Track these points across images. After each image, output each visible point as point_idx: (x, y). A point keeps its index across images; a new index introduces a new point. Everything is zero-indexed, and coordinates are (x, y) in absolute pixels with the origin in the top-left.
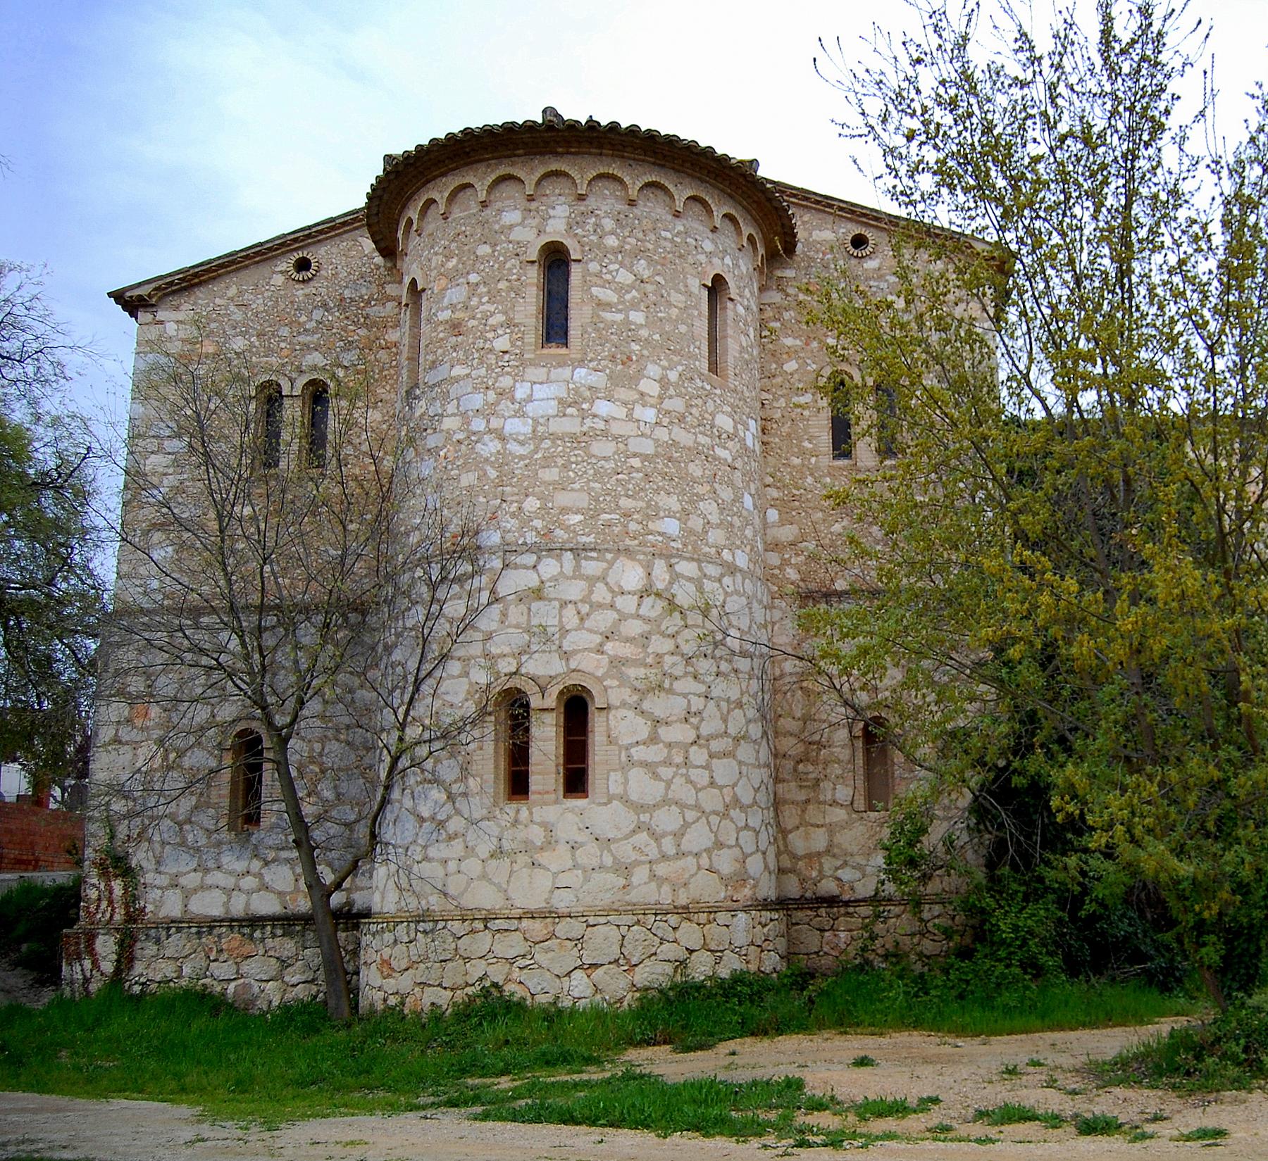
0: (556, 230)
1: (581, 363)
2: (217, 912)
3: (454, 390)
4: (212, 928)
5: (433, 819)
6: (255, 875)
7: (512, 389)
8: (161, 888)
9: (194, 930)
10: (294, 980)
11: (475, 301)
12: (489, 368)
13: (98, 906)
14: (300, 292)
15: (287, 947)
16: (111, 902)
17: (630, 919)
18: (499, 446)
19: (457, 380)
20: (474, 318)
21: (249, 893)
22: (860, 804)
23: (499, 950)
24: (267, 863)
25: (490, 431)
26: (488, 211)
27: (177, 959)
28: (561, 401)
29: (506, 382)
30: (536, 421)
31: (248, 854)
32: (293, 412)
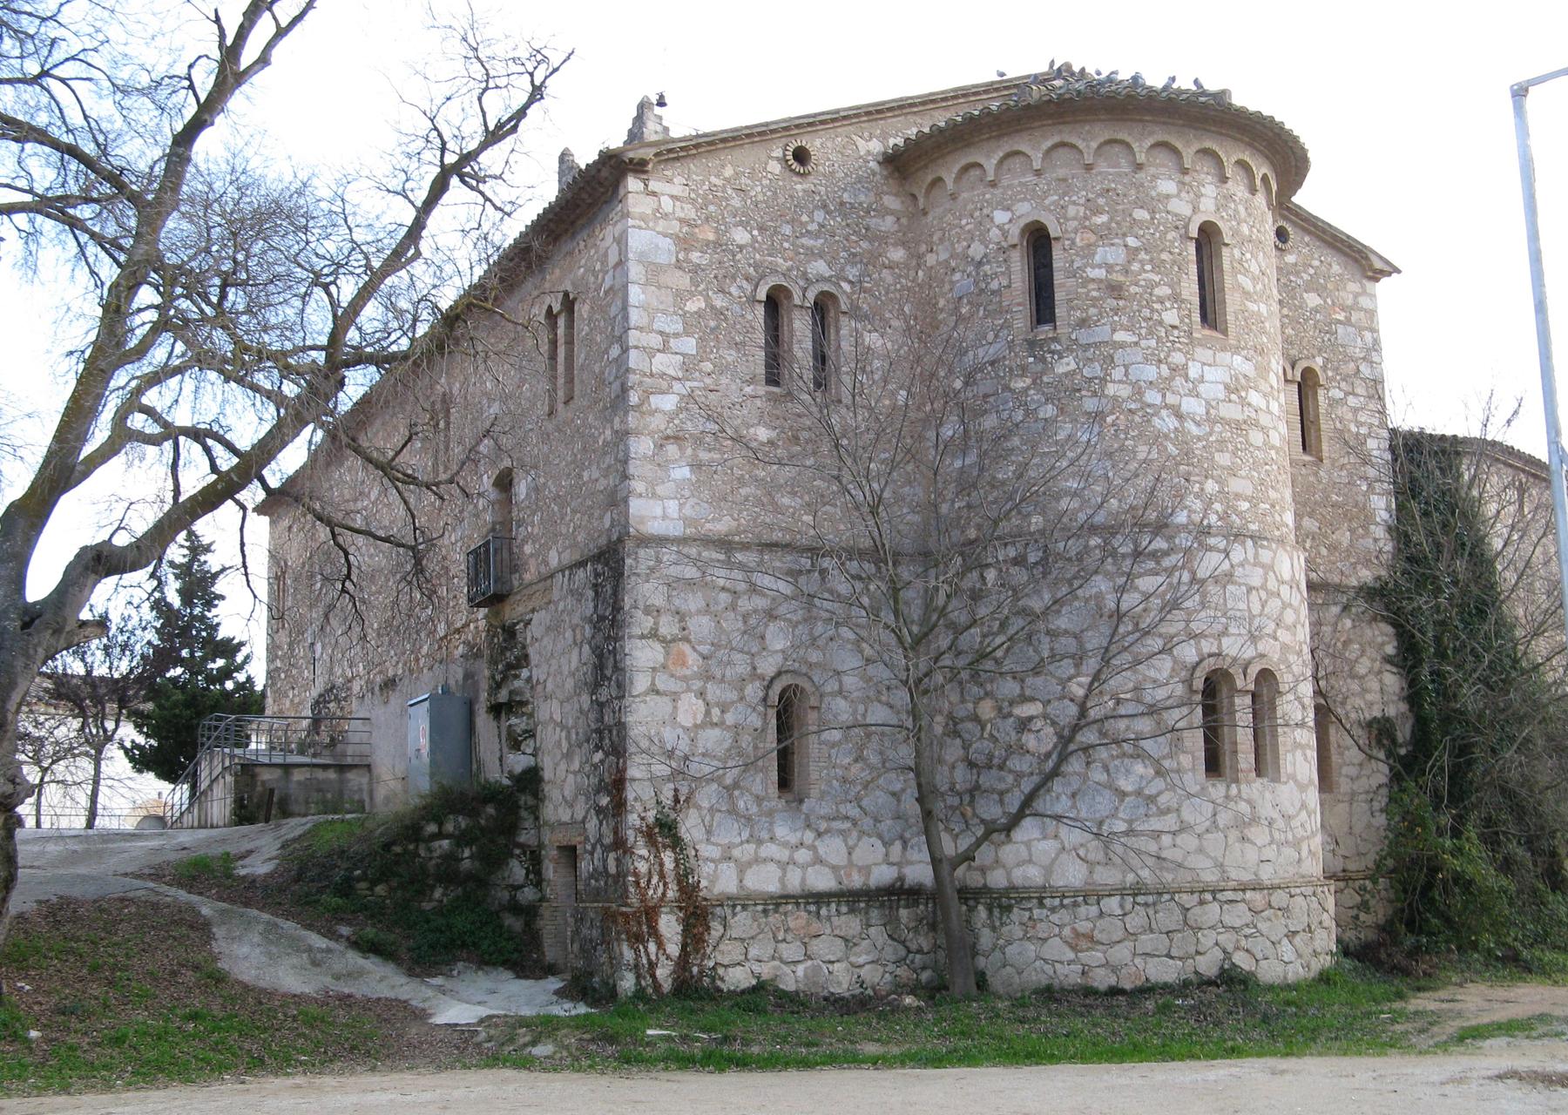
0: (1208, 210)
1: (1236, 350)
2: (773, 887)
3: (1118, 355)
4: (778, 905)
5: (1139, 793)
6: (808, 848)
7: (1185, 367)
8: (713, 861)
9: (760, 908)
10: (861, 960)
11: (1135, 267)
12: (1159, 339)
13: (649, 881)
14: (800, 187)
15: (850, 924)
16: (662, 876)
17: (1309, 891)
18: (1177, 424)
19: (1122, 345)
20: (1136, 284)
21: (804, 867)
23: (1227, 920)
24: (819, 835)
25: (1166, 406)
26: (1141, 175)
27: (742, 940)
28: (1227, 387)
29: (1177, 358)
30: (1208, 403)
31: (800, 823)
32: (800, 327)
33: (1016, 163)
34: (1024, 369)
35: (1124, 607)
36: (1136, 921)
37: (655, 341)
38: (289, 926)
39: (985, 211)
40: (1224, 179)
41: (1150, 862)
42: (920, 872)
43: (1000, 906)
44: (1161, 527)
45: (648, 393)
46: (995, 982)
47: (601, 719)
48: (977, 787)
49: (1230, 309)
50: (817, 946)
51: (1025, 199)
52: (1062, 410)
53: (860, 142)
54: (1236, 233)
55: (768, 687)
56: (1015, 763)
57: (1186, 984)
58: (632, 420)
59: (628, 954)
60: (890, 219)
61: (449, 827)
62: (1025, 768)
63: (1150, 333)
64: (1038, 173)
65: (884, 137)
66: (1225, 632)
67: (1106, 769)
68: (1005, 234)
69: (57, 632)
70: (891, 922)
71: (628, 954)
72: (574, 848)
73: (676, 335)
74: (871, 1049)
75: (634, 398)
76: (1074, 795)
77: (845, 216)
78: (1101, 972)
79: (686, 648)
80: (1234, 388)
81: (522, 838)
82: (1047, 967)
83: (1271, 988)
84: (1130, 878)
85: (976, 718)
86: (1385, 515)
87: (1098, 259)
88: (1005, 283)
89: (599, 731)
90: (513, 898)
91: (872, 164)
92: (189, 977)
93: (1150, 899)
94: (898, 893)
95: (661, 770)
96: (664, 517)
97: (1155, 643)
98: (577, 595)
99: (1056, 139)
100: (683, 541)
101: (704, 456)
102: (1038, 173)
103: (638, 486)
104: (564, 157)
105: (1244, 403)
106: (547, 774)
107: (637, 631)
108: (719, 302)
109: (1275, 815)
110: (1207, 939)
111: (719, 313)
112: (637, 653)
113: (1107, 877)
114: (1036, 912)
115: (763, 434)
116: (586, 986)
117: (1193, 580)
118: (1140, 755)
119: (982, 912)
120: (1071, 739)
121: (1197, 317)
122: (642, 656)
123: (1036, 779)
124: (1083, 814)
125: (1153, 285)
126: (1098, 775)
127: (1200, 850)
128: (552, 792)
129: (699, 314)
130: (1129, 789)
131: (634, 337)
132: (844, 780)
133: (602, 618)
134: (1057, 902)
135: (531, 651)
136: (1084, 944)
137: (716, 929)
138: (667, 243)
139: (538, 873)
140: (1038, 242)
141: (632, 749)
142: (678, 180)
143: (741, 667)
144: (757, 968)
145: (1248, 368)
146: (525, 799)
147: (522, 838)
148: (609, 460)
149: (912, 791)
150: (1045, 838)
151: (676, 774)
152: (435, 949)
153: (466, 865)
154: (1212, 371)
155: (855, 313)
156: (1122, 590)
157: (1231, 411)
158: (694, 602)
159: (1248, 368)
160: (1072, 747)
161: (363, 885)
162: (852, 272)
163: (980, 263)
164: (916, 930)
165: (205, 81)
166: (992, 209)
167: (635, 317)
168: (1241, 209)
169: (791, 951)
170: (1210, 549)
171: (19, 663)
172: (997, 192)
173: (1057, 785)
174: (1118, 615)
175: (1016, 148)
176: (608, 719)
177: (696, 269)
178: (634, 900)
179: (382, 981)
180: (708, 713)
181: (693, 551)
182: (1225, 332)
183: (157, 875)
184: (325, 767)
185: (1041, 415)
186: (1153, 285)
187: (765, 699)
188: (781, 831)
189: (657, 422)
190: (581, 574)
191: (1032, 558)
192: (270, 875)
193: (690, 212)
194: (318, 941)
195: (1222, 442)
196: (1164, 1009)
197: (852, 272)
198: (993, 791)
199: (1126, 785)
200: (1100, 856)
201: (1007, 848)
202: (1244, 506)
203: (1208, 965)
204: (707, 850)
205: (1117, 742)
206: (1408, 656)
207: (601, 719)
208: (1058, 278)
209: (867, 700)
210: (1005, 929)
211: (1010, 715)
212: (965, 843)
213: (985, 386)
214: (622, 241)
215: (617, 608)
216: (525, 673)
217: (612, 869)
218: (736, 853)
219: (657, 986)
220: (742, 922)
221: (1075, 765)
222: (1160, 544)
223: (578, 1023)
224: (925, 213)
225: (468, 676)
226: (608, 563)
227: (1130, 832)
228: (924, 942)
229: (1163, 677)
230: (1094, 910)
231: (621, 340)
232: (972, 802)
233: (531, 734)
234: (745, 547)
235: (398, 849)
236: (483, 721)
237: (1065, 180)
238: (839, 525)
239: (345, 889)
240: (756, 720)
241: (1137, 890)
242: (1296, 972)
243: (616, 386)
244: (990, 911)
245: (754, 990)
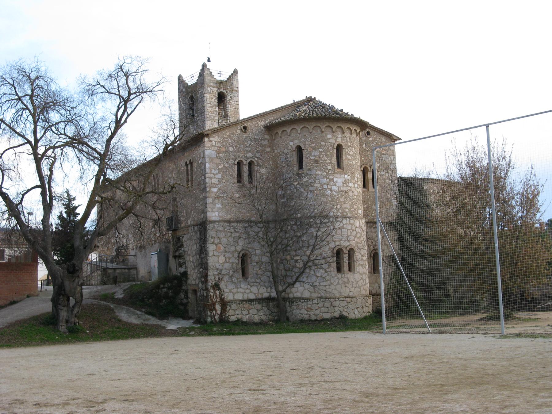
0: (339, 140)
1: (346, 174)
2: (241, 298)
5: (321, 276)
10: (261, 314)
11: (321, 156)
15: (259, 306)
16: (216, 296)
17: (362, 298)
19: (318, 175)
21: (248, 294)
22: (373, 272)
23: (341, 304)
24: (251, 286)
26: (323, 134)
28: (343, 183)
29: (331, 177)
31: (247, 283)
32: (245, 169)
33: (294, 131)
34: (296, 180)
35: (318, 235)
36: (321, 305)
37: (212, 176)
38: (131, 309)
40: (344, 133)
41: (324, 292)
42: (274, 294)
44: (327, 216)
45: (211, 188)
46: (291, 319)
47: (202, 261)
48: (287, 275)
49: (344, 164)
50: (251, 311)
53: (259, 123)
54: (347, 145)
55: (239, 254)
57: (332, 318)
58: (207, 195)
59: (209, 313)
60: (266, 141)
61: (166, 286)
63: (325, 171)
64: (299, 134)
65: (265, 121)
66: (341, 240)
67: (314, 271)
68: (292, 147)
69: (91, 249)
70: (268, 306)
71: (209, 313)
72: (196, 290)
73: (217, 174)
74: (260, 331)
75: (208, 189)
77: (256, 142)
79: (220, 245)
80: (345, 183)
81: (183, 288)
83: (351, 319)
84: (319, 295)
85: (286, 259)
86: (396, 203)
89: (202, 264)
90: (181, 302)
91: (262, 128)
92: (113, 320)
94: (269, 299)
95: (216, 273)
96: (215, 216)
97: (325, 243)
98: (196, 232)
99: (303, 126)
100: (219, 221)
101: (224, 202)
102: (299, 134)
103: (209, 209)
104: (181, 80)
105: (347, 186)
106: (189, 273)
107: (210, 242)
108: (226, 165)
109: (353, 281)
110: (336, 309)
111: (227, 168)
113: (314, 295)
115: (237, 195)
116: (199, 321)
117: (334, 228)
118: (322, 268)
119: (288, 303)
120: (306, 264)
121: (336, 167)
122: (211, 248)
123: (299, 273)
125: (325, 160)
126: (312, 272)
127: (335, 289)
128: (190, 278)
129: (222, 168)
131: (207, 175)
132: (257, 274)
133: (202, 239)
135: (184, 244)
136: (309, 310)
137: (228, 308)
138: (214, 153)
139: (187, 296)
140: (299, 150)
141: (209, 268)
143: (233, 249)
144: (237, 316)
145: (349, 178)
146: (184, 279)
147: (183, 288)
148: (202, 202)
149: (272, 277)
151: (219, 273)
152: (165, 315)
153: (170, 294)
154: (339, 180)
155: (258, 165)
156: (317, 231)
157: (345, 189)
158: (222, 235)
159: (349, 178)
161: (146, 300)
162: (258, 155)
163: (286, 154)
164: (274, 307)
165: (113, 126)
166: (290, 141)
167: (207, 170)
168: (348, 139)
169: (245, 312)
170: (338, 221)
171: (84, 256)
173: (304, 275)
174: (317, 237)
176: (204, 261)
177: (221, 158)
178: (210, 302)
179: (154, 321)
180: (226, 260)
181: (222, 224)
182: (343, 170)
183: (95, 298)
184: (125, 269)
186: (325, 160)
187: (238, 256)
188: (242, 286)
189: (213, 195)
190: (196, 228)
191: (298, 224)
192: (123, 298)
193: (219, 145)
194: (139, 313)
195: (342, 196)
196: (325, 324)
197: (258, 155)
198: (290, 276)
199: (319, 275)
200: (313, 291)
202: (347, 210)
203: (337, 315)
204: (226, 290)
205: (317, 265)
206: (401, 240)
207: (202, 261)
208: (304, 158)
209: (262, 256)
212: (284, 287)
213: (288, 183)
214: (204, 152)
215: (205, 237)
216: (183, 249)
217: (205, 294)
218: (232, 291)
219: (215, 320)
220: (234, 306)
221: (307, 270)
222: (326, 220)
223: (198, 328)
225: (166, 247)
226: (203, 226)
227: (320, 285)
228: (276, 310)
229: (327, 250)
230: (311, 302)
231: (205, 175)
232: (286, 279)
233: (184, 263)
234: (233, 222)
235: (154, 291)
236: (171, 259)
239: (142, 300)
240: (235, 260)
241: (321, 298)
242: (358, 316)
243: (203, 186)
245: (237, 321)
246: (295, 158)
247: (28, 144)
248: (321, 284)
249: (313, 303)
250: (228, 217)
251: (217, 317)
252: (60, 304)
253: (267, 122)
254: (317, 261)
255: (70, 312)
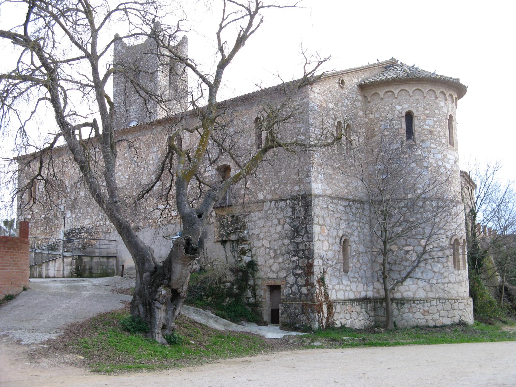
5: (439, 272)
11: (436, 126)
15: (358, 308)
16: (322, 295)
19: (433, 148)
39: (393, 105)
43: (401, 303)
51: (406, 104)
52: (417, 165)
56: (404, 263)
57: (452, 325)
62: (407, 264)
64: (411, 97)
65: (358, 78)
67: (431, 265)
76: (422, 272)
78: (431, 321)
82: (416, 320)
84: (437, 296)
87: (427, 123)
88: (400, 127)
91: (356, 86)
93: (444, 301)
94: (366, 300)
99: (416, 88)
102: (411, 97)
112: (315, 229)
113: (431, 295)
114: (412, 305)
119: (394, 305)
124: (425, 278)
125: (439, 132)
130: (437, 271)
134: (419, 302)
136: (426, 314)
139: (255, 294)
140: (409, 117)
142: (318, 88)
150: (414, 284)
160: (421, 259)
163: (391, 120)
172: (398, 100)
173: (417, 270)
175: (404, 88)
185: (411, 166)
186: (439, 132)
198: (397, 271)
200: (430, 290)
201: (402, 287)
203: (456, 320)
204: (330, 287)
205: (434, 258)
210: (402, 310)
211: (402, 249)
216: (246, 231)
221: (422, 264)
224: (369, 102)
230: (429, 304)
233: (250, 250)
237: (418, 100)
238: (361, 193)
241: (439, 299)
244: (397, 304)
246: (403, 125)
247: (87, 60)
248: (439, 281)
249: (431, 305)
250: (329, 192)
251: (324, 322)
252: (156, 300)
253: (360, 79)
254: (434, 253)
255: (170, 312)
